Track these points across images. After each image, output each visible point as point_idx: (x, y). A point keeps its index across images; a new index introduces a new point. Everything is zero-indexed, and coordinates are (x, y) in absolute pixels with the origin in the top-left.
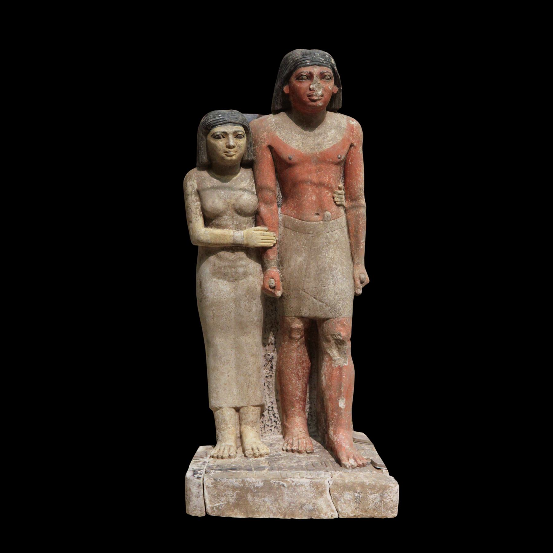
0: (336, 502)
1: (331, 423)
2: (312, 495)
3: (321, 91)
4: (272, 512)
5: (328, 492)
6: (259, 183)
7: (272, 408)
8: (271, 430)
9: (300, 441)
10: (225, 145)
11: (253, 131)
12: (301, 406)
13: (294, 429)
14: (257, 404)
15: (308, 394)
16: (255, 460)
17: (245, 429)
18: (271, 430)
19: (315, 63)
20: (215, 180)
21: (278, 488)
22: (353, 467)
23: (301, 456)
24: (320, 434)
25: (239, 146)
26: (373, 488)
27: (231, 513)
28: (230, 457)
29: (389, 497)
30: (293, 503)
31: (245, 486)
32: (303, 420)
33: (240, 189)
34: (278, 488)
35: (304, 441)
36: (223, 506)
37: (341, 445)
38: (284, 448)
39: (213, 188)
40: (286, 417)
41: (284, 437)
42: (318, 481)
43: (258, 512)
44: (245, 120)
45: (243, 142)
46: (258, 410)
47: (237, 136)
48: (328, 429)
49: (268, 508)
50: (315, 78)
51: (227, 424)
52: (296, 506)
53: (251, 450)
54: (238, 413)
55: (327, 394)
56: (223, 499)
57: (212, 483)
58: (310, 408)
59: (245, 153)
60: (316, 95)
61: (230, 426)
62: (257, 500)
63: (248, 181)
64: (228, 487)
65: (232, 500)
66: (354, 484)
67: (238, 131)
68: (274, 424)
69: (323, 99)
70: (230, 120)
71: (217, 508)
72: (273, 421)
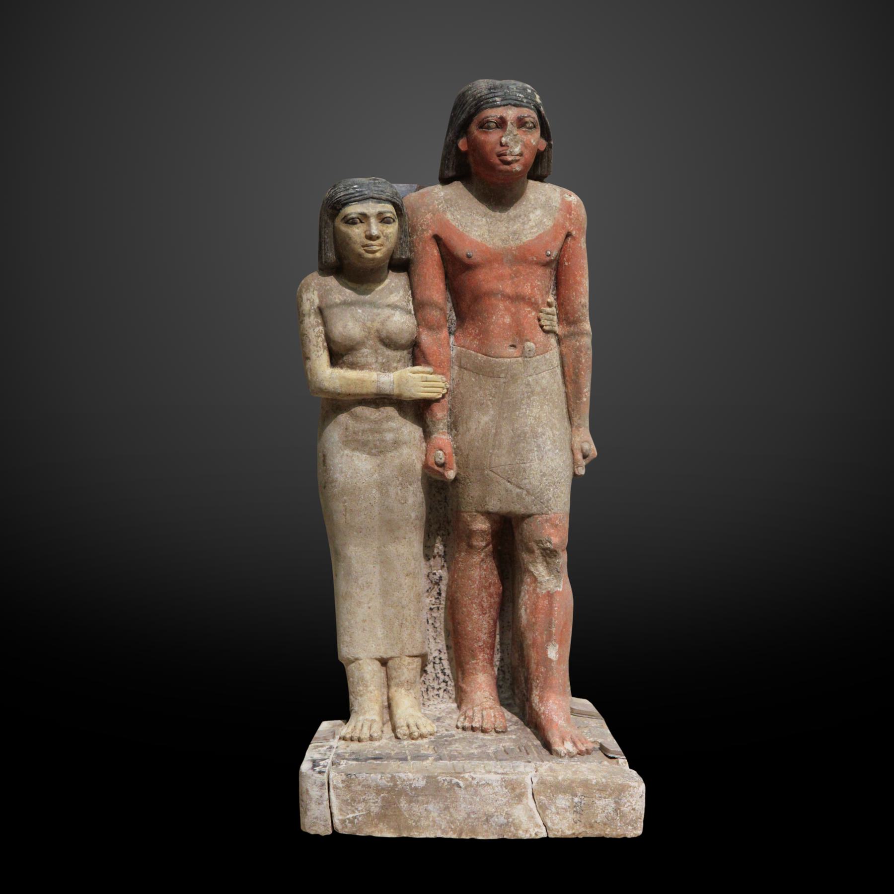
0: (544, 812)
1: (534, 684)
2: (505, 800)
3: (519, 147)
4: (440, 828)
5: (530, 796)
6: (418, 297)
7: (440, 659)
8: (438, 695)
9: (485, 713)
10: (363, 235)
11: (409, 213)
12: (486, 656)
13: (476, 693)
14: (415, 653)
15: (498, 637)
16: (413, 744)
17: (396, 694)
18: (438, 695)
19: (510, 101)
20: (348, 291)
21: (450, 789)
22: (570, 756)
23: (487, 737)
24: (518, 701)
25: (387, 237)
26: (603, 789)
27: (373, 829)
28: (371, 738)
29: (628, 804)
30: (474, 813)
31: (395, 785)
32: (490, 678)
33: (389, 306)
34: (450, 789)
35: (492, 712)
36: (360, 819)
37: (552, 720)
38: (460, 725)
39: (345, 303)
40: (463, 674)
41: (459, 707)
42: (515, 777)
43: (417, 827)
44: (397, 193)
45: (392, 229)
46: (417, 662)
47: (383, 219)
48: (531, 694)
49: (434, 821)
50: (509, 127)
51: (367, 686)
52: (478, 818)
53: (406, 728)
54: (384, 668)
55: (529, 637)
56: (361, 806)
57: (343, 781)
58: (502, 660)
59: (396, 248)
60: (511, 154)
61: (371, 688)
62: (416, 808)
63: (402, 293)
64: (369, 787)
65: (375, 809)
66: (573, 782)
67: (385, 212)
68: (443, 685)
69: (522, 160)
70: (371, 195)
71: (351, 821)
72: (441, 680)
